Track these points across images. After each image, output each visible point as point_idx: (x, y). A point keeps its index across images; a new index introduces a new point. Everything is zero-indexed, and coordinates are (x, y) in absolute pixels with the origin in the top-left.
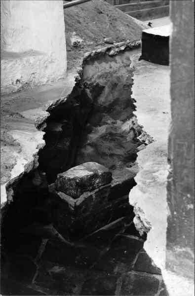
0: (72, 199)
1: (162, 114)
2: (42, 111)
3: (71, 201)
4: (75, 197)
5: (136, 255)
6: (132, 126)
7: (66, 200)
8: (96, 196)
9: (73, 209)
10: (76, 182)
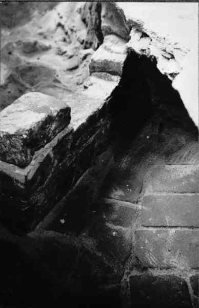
0: (18, 171)
1: (177, 42)
2: (89, 92)
3: (20, 174)
4: (22, 165)
5: (79, 184)
6: (58, 20)
7: (8, 172)
8: (54, 154)
9: (22, 187)
10: (24, 140)
